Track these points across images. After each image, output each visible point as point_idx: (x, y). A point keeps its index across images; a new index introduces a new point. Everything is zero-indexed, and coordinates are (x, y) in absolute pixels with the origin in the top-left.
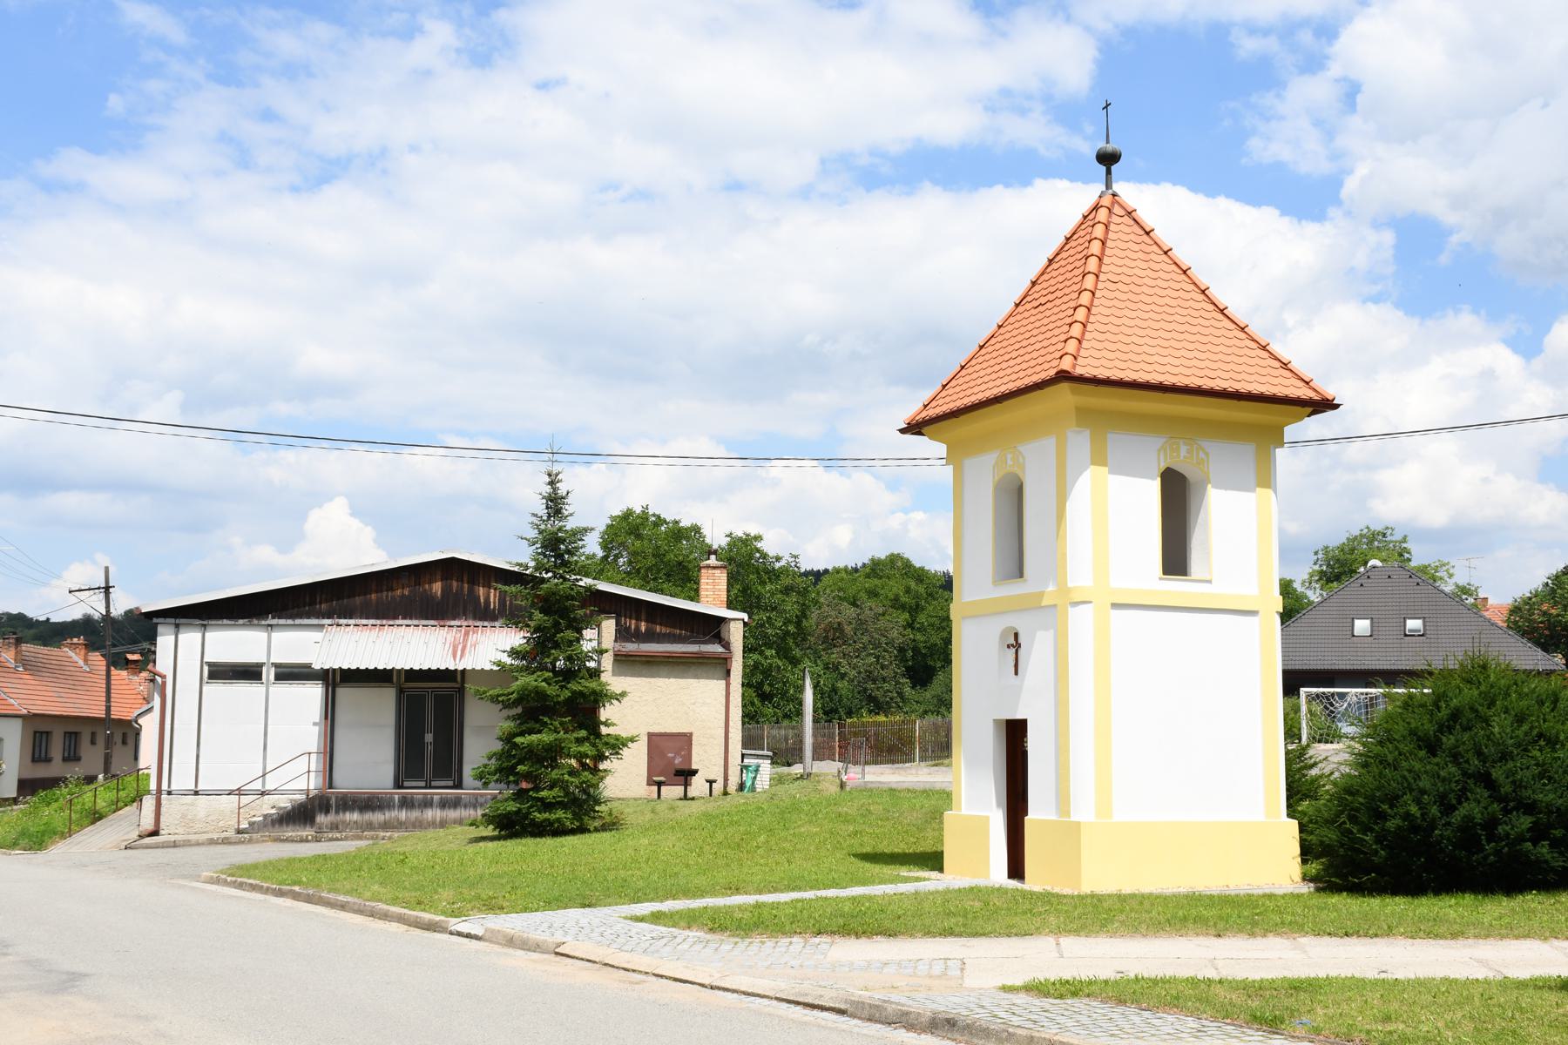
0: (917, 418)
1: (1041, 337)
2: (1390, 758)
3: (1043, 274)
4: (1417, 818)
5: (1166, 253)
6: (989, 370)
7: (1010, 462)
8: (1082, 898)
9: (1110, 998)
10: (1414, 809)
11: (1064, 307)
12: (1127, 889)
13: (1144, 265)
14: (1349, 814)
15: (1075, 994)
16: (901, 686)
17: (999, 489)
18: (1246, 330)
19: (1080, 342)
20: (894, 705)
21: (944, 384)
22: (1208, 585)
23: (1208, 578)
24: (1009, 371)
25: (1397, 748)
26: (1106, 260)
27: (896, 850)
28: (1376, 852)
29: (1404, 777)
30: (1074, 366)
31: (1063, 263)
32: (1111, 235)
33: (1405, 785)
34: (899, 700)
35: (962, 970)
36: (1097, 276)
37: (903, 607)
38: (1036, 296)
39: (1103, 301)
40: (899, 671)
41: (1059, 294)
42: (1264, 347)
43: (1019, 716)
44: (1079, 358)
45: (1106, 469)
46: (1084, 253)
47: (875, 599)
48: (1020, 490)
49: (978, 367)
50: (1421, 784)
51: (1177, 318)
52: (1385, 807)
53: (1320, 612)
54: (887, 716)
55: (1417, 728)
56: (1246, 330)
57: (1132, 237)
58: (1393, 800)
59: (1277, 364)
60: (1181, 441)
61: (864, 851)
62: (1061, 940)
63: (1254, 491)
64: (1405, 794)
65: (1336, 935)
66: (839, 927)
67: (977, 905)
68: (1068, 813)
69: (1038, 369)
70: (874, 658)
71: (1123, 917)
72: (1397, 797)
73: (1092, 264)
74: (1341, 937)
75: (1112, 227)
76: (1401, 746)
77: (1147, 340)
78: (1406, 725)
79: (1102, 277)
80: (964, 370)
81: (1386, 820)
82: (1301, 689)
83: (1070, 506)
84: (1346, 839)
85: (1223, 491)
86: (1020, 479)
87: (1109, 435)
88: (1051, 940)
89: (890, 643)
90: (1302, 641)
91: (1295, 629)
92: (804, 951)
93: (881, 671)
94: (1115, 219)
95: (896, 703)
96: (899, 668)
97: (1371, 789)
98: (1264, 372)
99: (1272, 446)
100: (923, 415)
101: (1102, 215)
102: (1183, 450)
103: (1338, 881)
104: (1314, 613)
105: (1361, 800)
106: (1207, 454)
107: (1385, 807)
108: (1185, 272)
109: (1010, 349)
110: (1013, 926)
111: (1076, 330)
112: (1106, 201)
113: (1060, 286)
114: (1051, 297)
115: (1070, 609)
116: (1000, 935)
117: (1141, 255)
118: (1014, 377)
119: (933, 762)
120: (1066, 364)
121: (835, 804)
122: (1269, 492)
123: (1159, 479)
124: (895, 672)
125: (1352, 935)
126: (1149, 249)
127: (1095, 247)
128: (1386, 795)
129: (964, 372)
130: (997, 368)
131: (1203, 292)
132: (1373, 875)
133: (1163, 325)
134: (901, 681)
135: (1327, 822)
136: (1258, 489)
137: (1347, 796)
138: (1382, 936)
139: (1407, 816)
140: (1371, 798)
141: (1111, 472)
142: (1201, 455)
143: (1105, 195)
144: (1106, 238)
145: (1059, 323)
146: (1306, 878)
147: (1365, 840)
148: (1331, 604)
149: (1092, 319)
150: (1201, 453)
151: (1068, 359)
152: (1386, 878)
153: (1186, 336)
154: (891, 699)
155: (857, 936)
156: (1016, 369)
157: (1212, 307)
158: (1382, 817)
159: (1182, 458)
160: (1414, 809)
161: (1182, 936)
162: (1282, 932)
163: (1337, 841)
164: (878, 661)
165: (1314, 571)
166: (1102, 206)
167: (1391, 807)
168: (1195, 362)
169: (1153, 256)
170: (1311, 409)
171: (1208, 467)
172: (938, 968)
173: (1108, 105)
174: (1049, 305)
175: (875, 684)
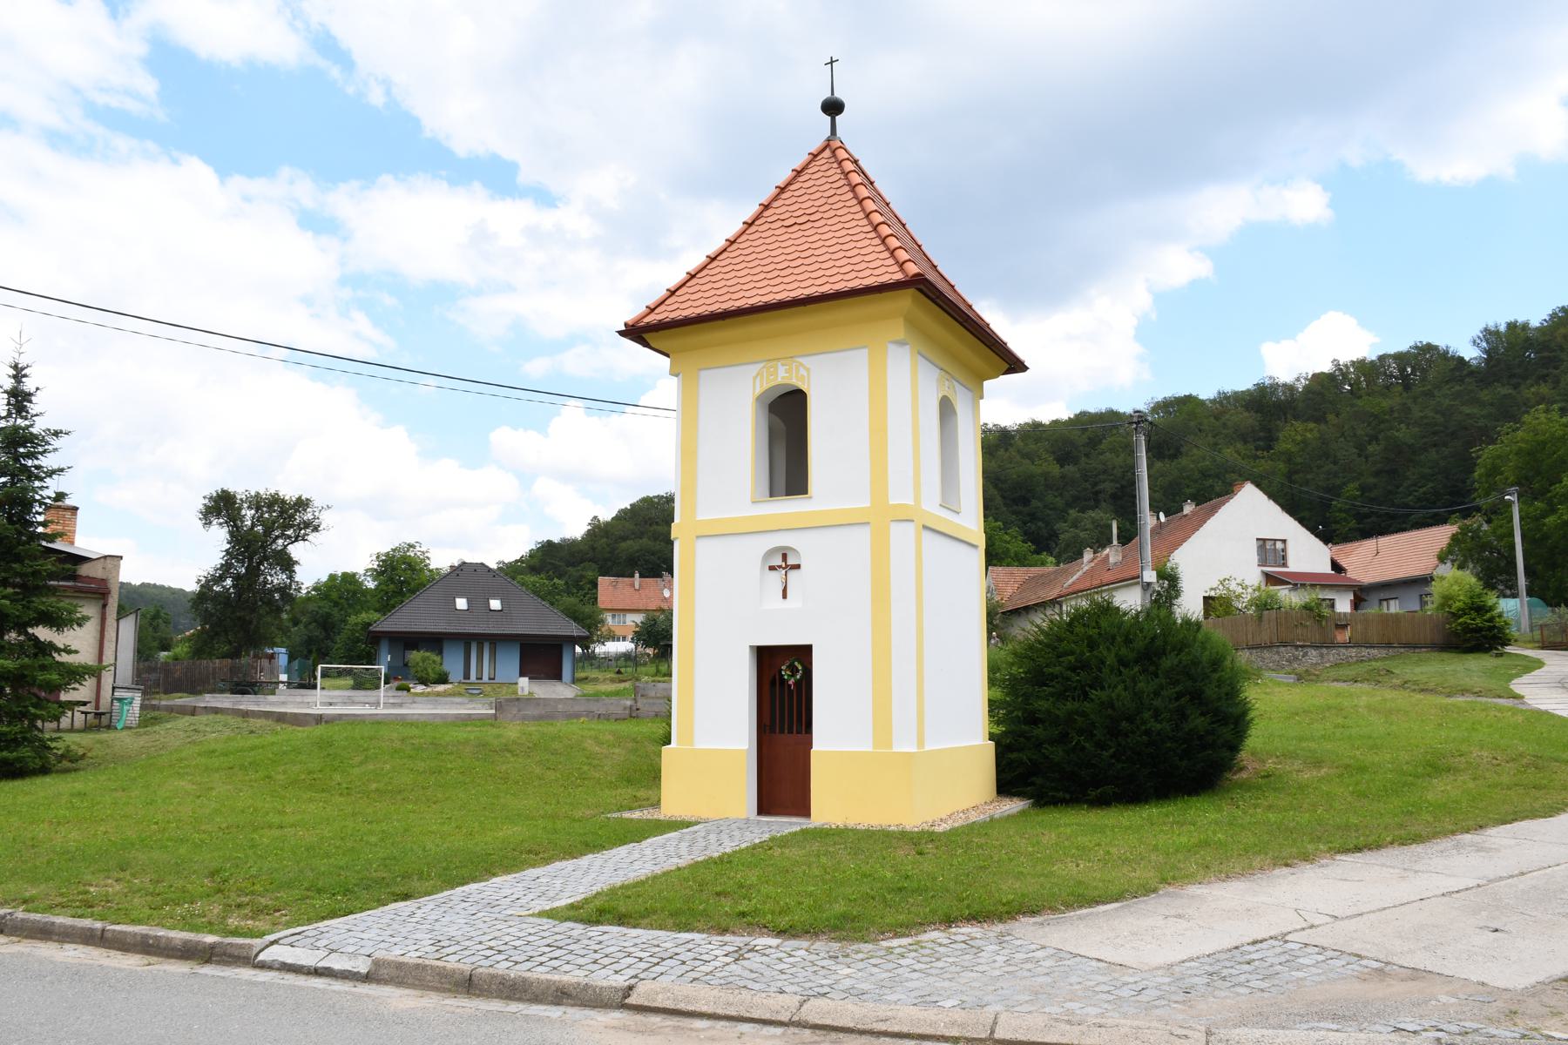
142: (803, 372)
150: (801, 369)
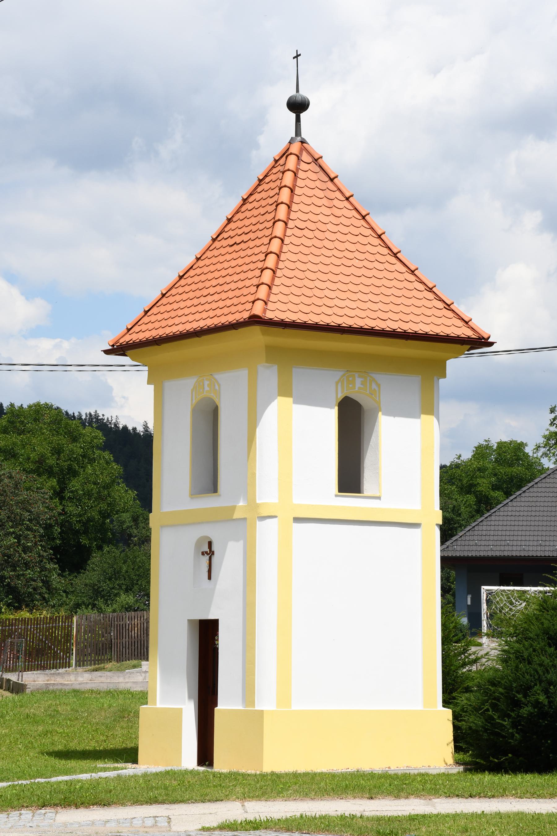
0: (121, 341)
1: (236, 278)
2: (526, 654)
3: (237, 212)
4: (544, 705)
5: (347, 199)
6: (189, 303)
7: (207, 388)
8: (263, 776)
9: (281, 828)
10: (542, 698)
11: (257, 250)
12: (301, 769)
13: (327, 211)
14: (492, 702)
15: (255, 829)
16: (47, 573)
17: (196, 411)
18: (416, 272)
19: (270, 288)
20: (38, 597)
21: (147, 309)
22: (378, 500)
23: (378, 495)
24: (207, 307)
25: (531, 646)
26: (294, 207)
27: (87, 748)
28: (512, 735)
29: (536, 670)
30: (265, 310)
31: (255, 204)
32: (299, 183)
33: (537, 677)
34: (44, 590)
35: (169, 822)
36: (286, 224)
37: (50, 473)
38: (232, 233)
39: (287, 264)
40: (45, 554)
41: (252, 236)
42: (431, 289)
43: (211, 617)
44: (269, 303)
45: (290, 400)
46: (278, 183)
47: (13, 460)
48: (215, 412)
49: (178, 298)
50: (549, 676)
51: (356, 262)
52: (520, 696)
53: (543, 490)
54: (31, 611)
55: (549, 628)
56: (416, 272)
57: (318, 184)
58: (526, 689)
59: (441, 305)
60: (357, 375)
61: (56, 749)
62: (246, 804)
63: (419, 417)
64: (536, 685)
65: (463, 796)
66: (60, 800)
67: (175, 783)
68: (253, 703)
69: (233, 309)
70: (15, 538)
71: (297, 787)
72: (530, 688)
73: (282, 211)
74: (467, 798)
75: (301, 174)
76: (535, 644)
77: (329, 284)
78: (540, 626)
79: (291, 224)
80: (164, 298)
81: (521, 707)
82: (483, 587)
83: (259, 431)
84: (489, 725)
85: (392, 418)
86: (214, 402)
87: (294, 370)
88: (238, 804)
89: (35, 519)
90: (521, 523)
91: (514, 509)
92: (34, 818)
93: (23, 555)
94: (303, 166)
95: (40, 594)
96: (45, 551)
97: (509, 681)
98: (428, 312)
99: (435, 378)
100: (127, 338)
101: (292, 162)
102: (358, 382)
103: (482, 762)
104: (535, 490)
105: (500, 690)
106: (379, 386)
107: (520, 696)
108: (364, 217)
109: (208, 284)
110: (207, 795)
111: (267, 276)
112: (295, 148)
113: (254, 228)
114: (245, 238)
115: (258, 523)
116: (196, 801)
117: (325, 201)
118: (211, 314)
119: (93, 667)
120: (258, 309)
121: (21, 706)
122: (432, 419)
123: (337, 408)
124: (39, 556)
125: (475, 796)
126: (332, 195)
127: (285, 195)
128: (521, 686)
129: (164, 301)
130: (196, 301)
131: (379, 236)
132: (510, 755)
133: (343, 269)
134: (48, 566)
135: (477, 709)
136: (422, 416)
137: (490, 687)
138: (498, 797)
139: (537, 704)
140: (509, 689)
141: (295, 402)
142: (374, 386)
143: (294, 142)
144: (295, 185)
145: (252, 266)
146: (458, 763)
147: (504, 726)
148: (548, 485)
149: (281, 265)
151: (259, 304)
152: (521, 758)
153: (363, 280)
154: (35, 589)
155: (77, 807)
156: (214, 305)
157: (385, 251)
158: (517, 704)
159: (357, 389)
160: (542, 698)
161: (342, 799)
162: (421, 795)
163: (483, 727)
164: (19, 542)
165: (551, 433)
166: (291, 154)
167: (525, 696)
168: (370, 305)
169: (336, 202)
170: (469, 347)
171: (379, 396)
172: (150, 822)
173: (298, 56)
174: (243, 246)
175: (14, 570)
